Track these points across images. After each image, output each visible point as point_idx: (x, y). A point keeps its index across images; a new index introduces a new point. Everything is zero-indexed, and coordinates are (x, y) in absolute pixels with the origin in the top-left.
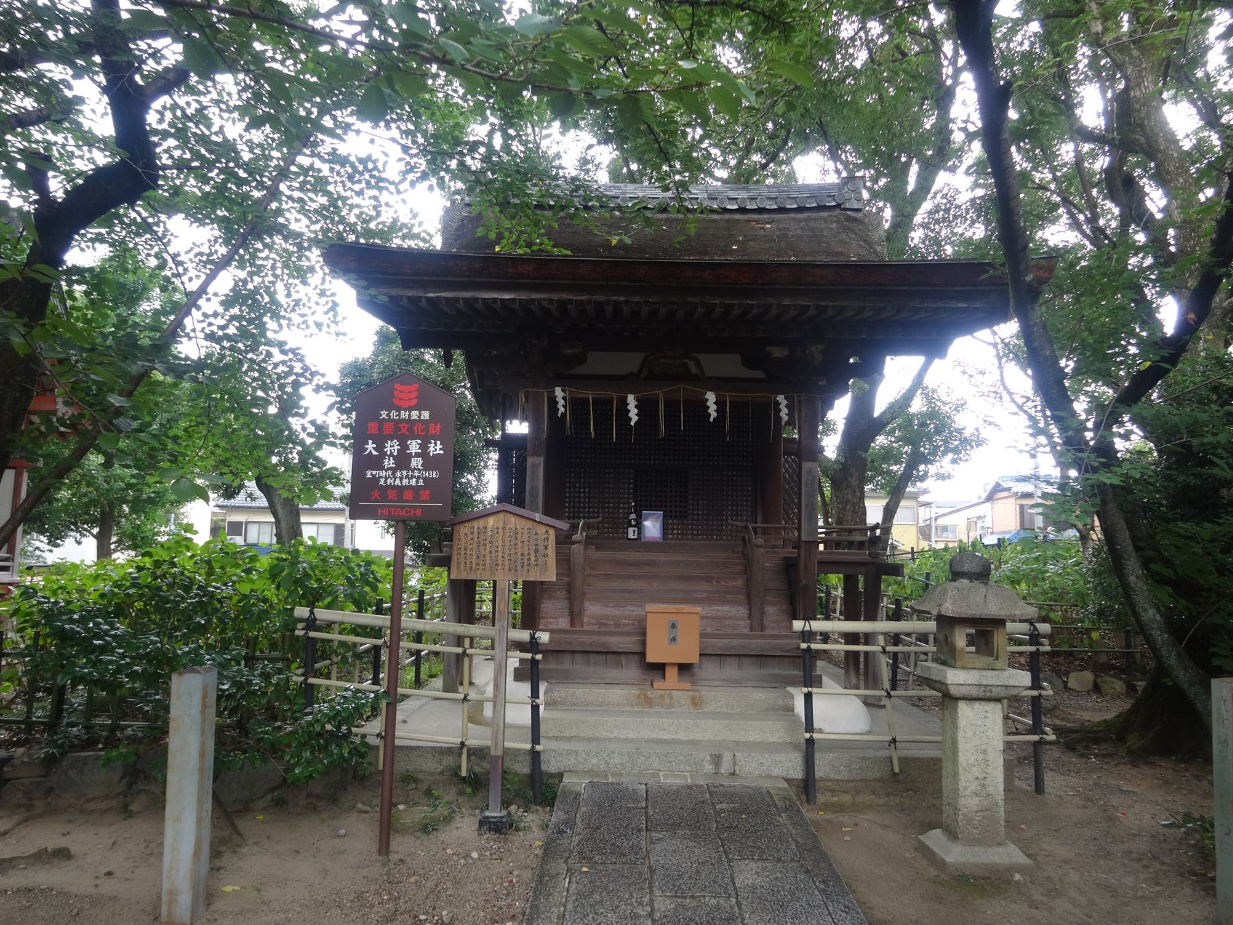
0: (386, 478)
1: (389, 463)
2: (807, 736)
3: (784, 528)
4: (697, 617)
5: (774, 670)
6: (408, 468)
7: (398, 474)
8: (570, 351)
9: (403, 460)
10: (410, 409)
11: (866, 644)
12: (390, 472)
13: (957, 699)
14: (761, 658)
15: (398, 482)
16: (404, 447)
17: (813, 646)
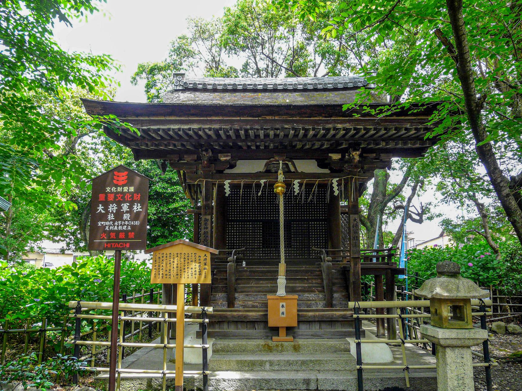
0: (109, 226)
1: (111, 217)
2: (358, 367)
3: (342, 251)
4: (296, 301)
5: (339, 329)
6: (122, 220)
7: (116, 223)
8: (225, 158)
9: (119, 215)
10: (123, 186)
11: (388, 313)
12: (112, 223)
13: (445, 347)
14: (332, 322)
15: (116, 228)
16: (120, 208)
17: (361, 316)
